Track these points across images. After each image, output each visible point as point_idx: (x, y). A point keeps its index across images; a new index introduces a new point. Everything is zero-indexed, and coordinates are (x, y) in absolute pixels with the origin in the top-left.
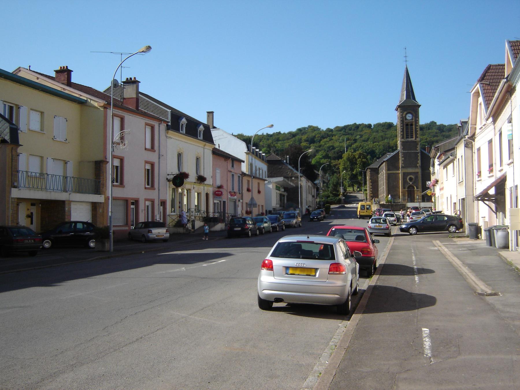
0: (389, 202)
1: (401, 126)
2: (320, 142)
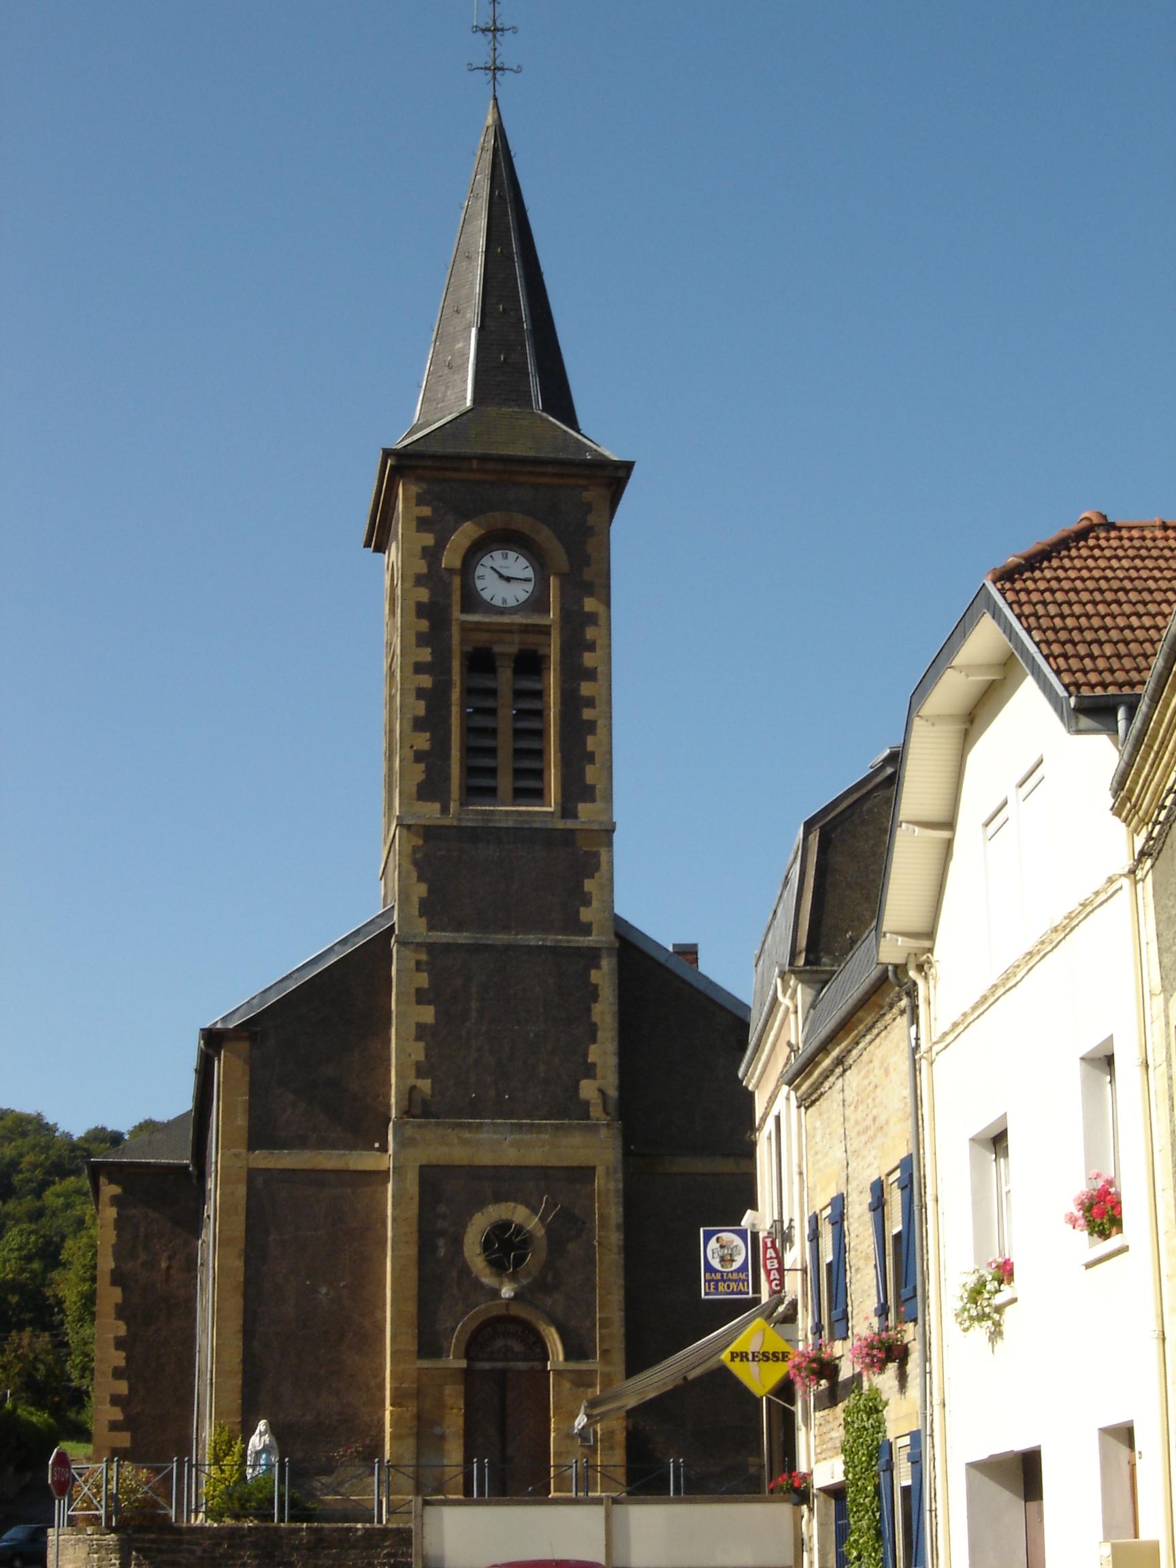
0: (244, 1500)
1: (419, 668)
2: (38, 1193)
